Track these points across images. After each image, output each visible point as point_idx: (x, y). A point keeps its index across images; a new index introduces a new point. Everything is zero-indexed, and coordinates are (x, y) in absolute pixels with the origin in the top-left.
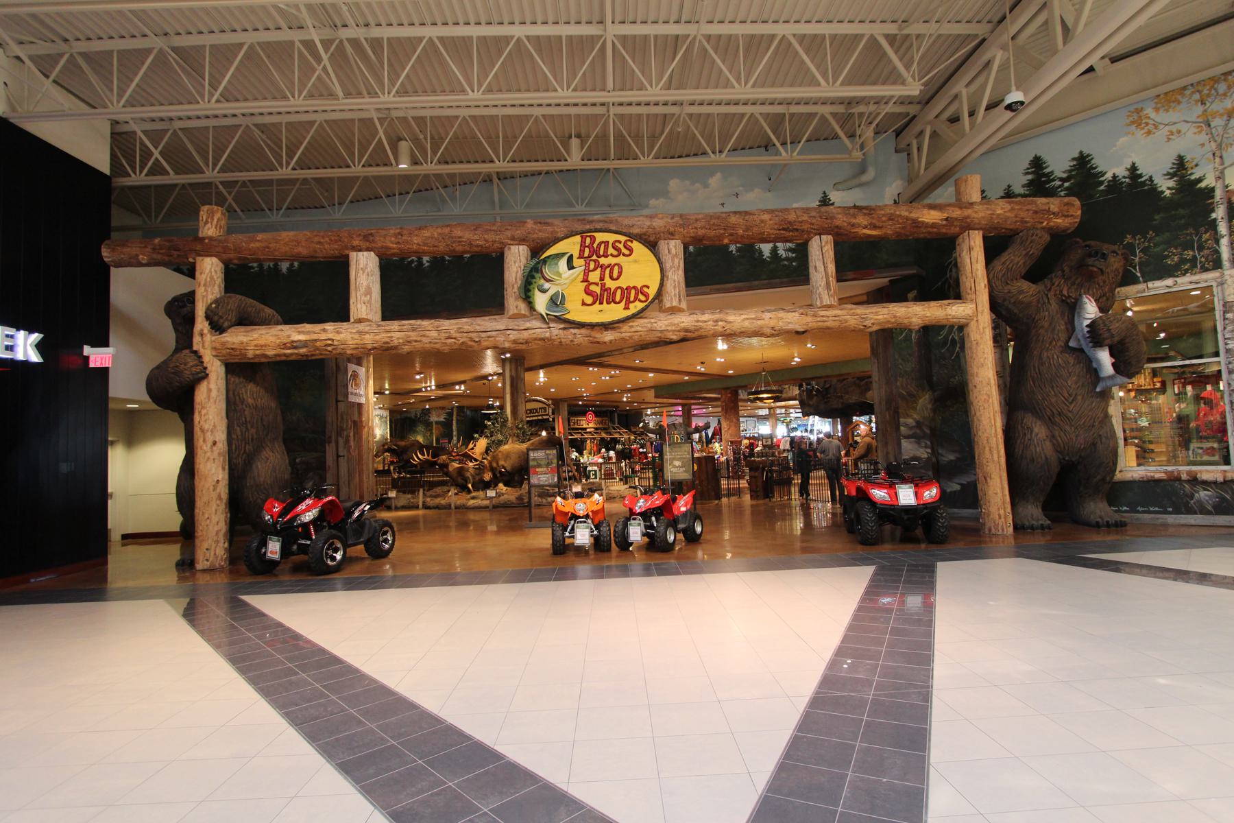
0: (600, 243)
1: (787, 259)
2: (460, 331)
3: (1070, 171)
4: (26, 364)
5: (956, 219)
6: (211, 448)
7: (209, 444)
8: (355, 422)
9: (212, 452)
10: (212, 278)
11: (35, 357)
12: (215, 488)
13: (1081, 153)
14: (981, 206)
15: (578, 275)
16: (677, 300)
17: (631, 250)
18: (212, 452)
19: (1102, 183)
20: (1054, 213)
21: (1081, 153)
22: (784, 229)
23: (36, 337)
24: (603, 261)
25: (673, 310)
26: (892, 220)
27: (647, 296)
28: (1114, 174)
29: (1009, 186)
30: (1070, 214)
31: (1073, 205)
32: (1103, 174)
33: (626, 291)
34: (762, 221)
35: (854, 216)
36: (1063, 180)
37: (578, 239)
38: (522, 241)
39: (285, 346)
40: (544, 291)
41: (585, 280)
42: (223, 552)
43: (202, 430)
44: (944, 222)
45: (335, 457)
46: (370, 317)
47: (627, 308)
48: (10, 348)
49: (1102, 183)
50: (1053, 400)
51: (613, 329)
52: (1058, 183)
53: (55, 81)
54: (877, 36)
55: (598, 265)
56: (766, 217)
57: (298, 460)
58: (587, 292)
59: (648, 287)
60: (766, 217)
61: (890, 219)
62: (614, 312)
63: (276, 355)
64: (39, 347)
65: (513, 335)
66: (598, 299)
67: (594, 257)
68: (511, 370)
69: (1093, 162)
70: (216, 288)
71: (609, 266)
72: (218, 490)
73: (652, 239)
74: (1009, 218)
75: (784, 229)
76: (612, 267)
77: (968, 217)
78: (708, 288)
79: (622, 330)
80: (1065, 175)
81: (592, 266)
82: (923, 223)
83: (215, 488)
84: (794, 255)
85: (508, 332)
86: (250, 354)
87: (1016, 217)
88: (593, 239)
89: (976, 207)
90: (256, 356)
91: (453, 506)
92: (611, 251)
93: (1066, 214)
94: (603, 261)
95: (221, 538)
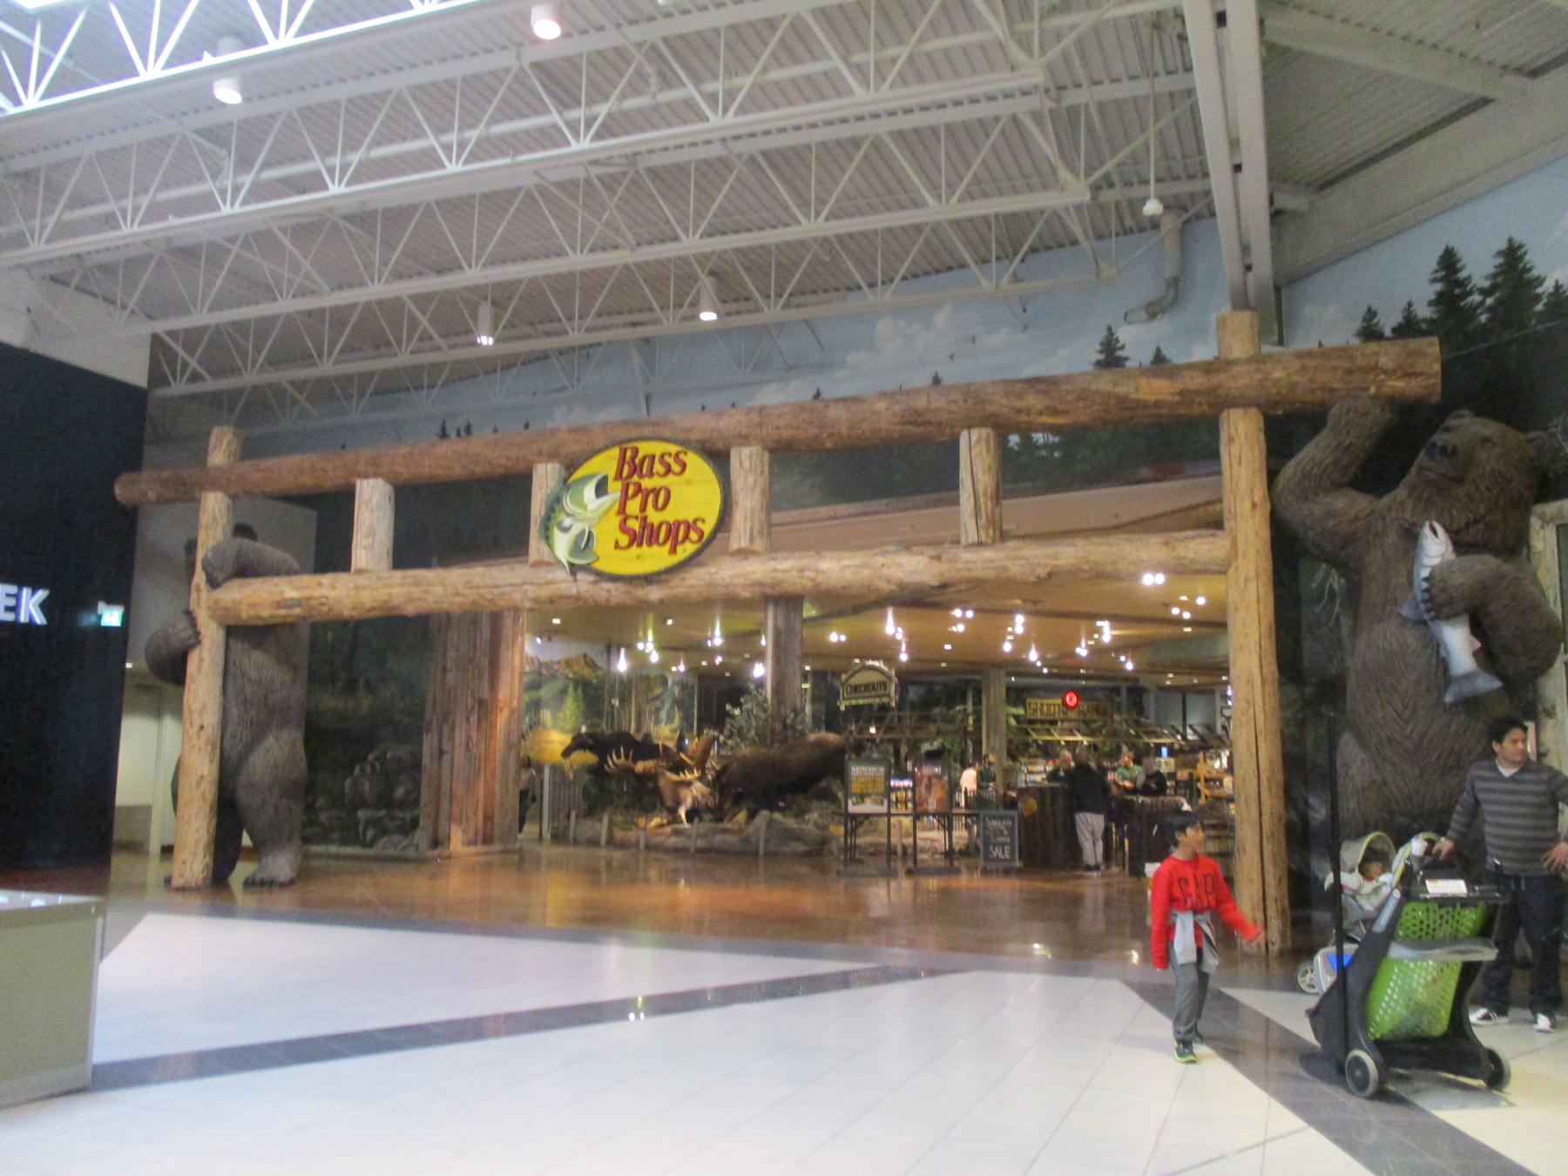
0: (644, 458)
1: (1046, 446)
2: (469, 585)
3: (1495, 276)
4: (31, 623)
5: (1198, 392)
6: (198, 733)
7: (196, 728)
8: (481, 703)
9: (198, 737)
10: (214, 518)
11: (40, 619)
12: (199, 784)
13: (1510, 240)
14: (1245, 367)
15: (611, 506)
16: (748, 538)
17: (684, 467)
18: (198, 737)
19: (1538, 298)
20: (1385, 372)
21: (1510, 240)
22: (909, 423)
23: (42, 594)
24: (647, 483)
25: (743, 553)
26: (1083, 399)
27: (701, 534)
28: (1557, 282)
29: (1410, 305)
30: (1418, 370)
31: (1425, 355)
33: (673, 529)
34: (875, 413)
35: (1020, 396)
36: (1485, 293)
37: (615, 452)
38: (551, 456)
39: (279, 604)
40: (566, 530)
41: (622, 509)
42: (201, 868)
43: (190, 711)
44: (1177, 398)
45: (436, 753)
46: (371, 566)
47: (673, 551)
48: (14, 609)
49: (1538, 298)
50: (1379, 715)
51: (659, 582)
52: (1477, 298)
53: (76, 288)
54: (1021, 116)
55: (639, 489)
56: (881, 406)
57: (389, 755)
58: (623, 528)
59: (704, 521)
60: (881, 406)
61: (1079, 398)
62: (656, 558)
63: (271, 617)
64: (44, 606)
65: (532, 591)
66: (635, 539)
67: (635, 478)
68: (775, 618)
69: (1527, 258)
70: (220, 531)
72: (202, 787)
73: (720, 445)
74: (1296, 384)
75: (909, 423)
76: (656, 492)
77: (1219, 386)
78: (920, 499)
79: (672, 584)
81: (631, 490)
82: (1138, 402)
83: (199, 784)
84: (1057, 439)
86: (244, 615)
87: (1311, 381)
88: (636, 451)
89: (1237, 369)
90: (251, 618)
91: (642, 844)
92: (658, 468)
93: (1411, 371)
94: (647, 483)
95: (201, 852)
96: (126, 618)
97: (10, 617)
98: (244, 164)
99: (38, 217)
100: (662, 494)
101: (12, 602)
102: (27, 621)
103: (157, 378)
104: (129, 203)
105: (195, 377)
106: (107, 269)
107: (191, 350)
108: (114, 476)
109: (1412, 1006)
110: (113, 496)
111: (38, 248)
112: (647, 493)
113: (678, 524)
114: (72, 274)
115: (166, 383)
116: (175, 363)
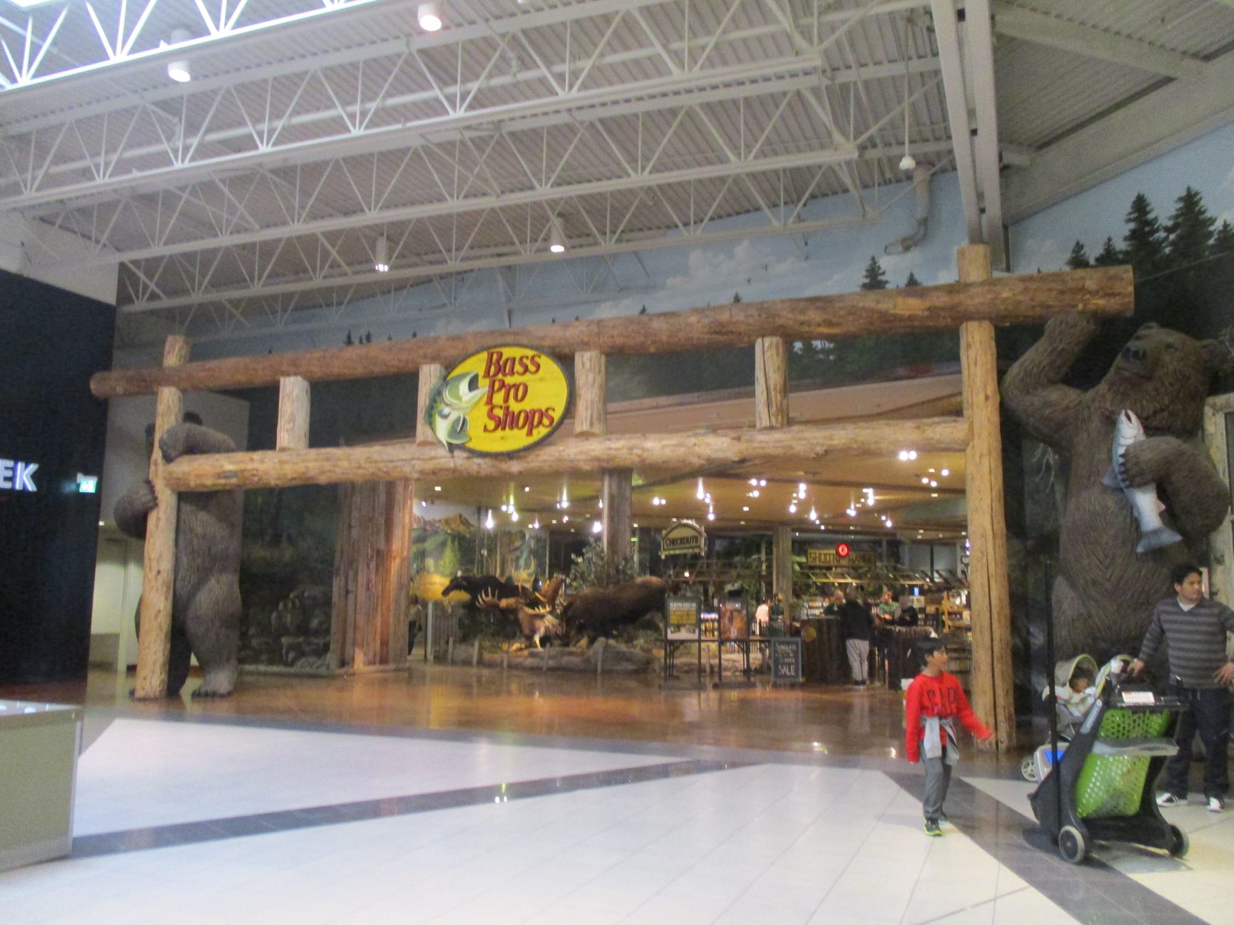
0: (507, 360)
1: (823, 351)
2: (369, 460)
3: (1177, 217)
4: (24, 490)
5: (943, 309)
6: (156, 577)
7: (154, 572)
8: (379, 553)
9: (156, 580)
10: (169, 407)
11: (31, 487)
12: (156, 617)
13: (1189, 189)
14: (980, 289)
15: (481, 398)
16: (588, 423)
17: (538, 367)
18: (156, 580)
19: (1210, 234)
20: (1090, 293)
21: (1189, 189)
22: (716, 332)
23: (33, 467)
24: (509, 380)
25: (585, 435)
26: (852, 314)
27: (552, 420)
28: (1225, 222)
29: (1110, 240)
30: (1116, 291)
31: (1122, 279)
32: (1212, 221)
33: (529, 416)
35: (803, 312)
36: (1169, 230)
37: (484, 355)
38: (434, 359)
39: (220, 475)
40: (445, 417)
41: (490, 401)
42: (158, 683)
45: (343, 593)
46: (292, 446)
48: (11, 479)
49: (1210, 234)
51: (519, 458)
52: (1162, 234)
53: (60, 227)
54: (803, 91)
55: (503, 385)
56: (693, 319)
57: (306, 594)
58: (491, 415)
59: (554, 410)
60: (693, 319)
61: (850, 313)
62: (516, 439)
63: (214, 485)
64: (35, 477)
65: (419, 465)
66: (500, 424)
67: (500, 376)
68: (610, 486)
69: (1202, 203)
70: (173, 418)
71: (514, 385)
72: (159, 619)
74: (1020, 302)
75: (716, 332)
76: (516, 387)
77: (960, 304)
78: (724, 392)
79: (529, 459)
80: (1170, 223)
81: (497, 386)
82: (895, 316)
83: (156, 617)
84: (832, 346)
85: (413, 462)
86: (192, 484)
87: (1032, 299)
88: (500, 355)
89: (973, 290)
90: (197, 486)
91: (505, 664)
92: (518, 368)
93: (1110, 292)
94: (509, 380)
95: (158, 670)
96: (99, 486)
97: (8, 485)
98: (192, 129)
99: (30, 171)
100: (521, 389)
101: (9, 474)
102: (21, 488)
103: (124, 297)
104: (101, 160)
105: (154, 297)
106: (84, 212)
107: (150, 276)
108: (89, 375)
109: (1111, 791)
110: (89, 390)
111: (30, 195)
112: (510, 388)
113: (534, 412)
114: (57, 215)
115: (130, 301)
116: (138, 285)
